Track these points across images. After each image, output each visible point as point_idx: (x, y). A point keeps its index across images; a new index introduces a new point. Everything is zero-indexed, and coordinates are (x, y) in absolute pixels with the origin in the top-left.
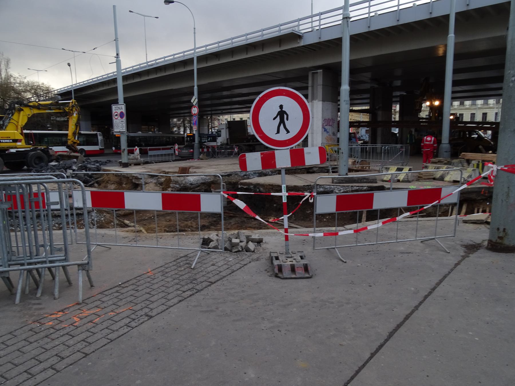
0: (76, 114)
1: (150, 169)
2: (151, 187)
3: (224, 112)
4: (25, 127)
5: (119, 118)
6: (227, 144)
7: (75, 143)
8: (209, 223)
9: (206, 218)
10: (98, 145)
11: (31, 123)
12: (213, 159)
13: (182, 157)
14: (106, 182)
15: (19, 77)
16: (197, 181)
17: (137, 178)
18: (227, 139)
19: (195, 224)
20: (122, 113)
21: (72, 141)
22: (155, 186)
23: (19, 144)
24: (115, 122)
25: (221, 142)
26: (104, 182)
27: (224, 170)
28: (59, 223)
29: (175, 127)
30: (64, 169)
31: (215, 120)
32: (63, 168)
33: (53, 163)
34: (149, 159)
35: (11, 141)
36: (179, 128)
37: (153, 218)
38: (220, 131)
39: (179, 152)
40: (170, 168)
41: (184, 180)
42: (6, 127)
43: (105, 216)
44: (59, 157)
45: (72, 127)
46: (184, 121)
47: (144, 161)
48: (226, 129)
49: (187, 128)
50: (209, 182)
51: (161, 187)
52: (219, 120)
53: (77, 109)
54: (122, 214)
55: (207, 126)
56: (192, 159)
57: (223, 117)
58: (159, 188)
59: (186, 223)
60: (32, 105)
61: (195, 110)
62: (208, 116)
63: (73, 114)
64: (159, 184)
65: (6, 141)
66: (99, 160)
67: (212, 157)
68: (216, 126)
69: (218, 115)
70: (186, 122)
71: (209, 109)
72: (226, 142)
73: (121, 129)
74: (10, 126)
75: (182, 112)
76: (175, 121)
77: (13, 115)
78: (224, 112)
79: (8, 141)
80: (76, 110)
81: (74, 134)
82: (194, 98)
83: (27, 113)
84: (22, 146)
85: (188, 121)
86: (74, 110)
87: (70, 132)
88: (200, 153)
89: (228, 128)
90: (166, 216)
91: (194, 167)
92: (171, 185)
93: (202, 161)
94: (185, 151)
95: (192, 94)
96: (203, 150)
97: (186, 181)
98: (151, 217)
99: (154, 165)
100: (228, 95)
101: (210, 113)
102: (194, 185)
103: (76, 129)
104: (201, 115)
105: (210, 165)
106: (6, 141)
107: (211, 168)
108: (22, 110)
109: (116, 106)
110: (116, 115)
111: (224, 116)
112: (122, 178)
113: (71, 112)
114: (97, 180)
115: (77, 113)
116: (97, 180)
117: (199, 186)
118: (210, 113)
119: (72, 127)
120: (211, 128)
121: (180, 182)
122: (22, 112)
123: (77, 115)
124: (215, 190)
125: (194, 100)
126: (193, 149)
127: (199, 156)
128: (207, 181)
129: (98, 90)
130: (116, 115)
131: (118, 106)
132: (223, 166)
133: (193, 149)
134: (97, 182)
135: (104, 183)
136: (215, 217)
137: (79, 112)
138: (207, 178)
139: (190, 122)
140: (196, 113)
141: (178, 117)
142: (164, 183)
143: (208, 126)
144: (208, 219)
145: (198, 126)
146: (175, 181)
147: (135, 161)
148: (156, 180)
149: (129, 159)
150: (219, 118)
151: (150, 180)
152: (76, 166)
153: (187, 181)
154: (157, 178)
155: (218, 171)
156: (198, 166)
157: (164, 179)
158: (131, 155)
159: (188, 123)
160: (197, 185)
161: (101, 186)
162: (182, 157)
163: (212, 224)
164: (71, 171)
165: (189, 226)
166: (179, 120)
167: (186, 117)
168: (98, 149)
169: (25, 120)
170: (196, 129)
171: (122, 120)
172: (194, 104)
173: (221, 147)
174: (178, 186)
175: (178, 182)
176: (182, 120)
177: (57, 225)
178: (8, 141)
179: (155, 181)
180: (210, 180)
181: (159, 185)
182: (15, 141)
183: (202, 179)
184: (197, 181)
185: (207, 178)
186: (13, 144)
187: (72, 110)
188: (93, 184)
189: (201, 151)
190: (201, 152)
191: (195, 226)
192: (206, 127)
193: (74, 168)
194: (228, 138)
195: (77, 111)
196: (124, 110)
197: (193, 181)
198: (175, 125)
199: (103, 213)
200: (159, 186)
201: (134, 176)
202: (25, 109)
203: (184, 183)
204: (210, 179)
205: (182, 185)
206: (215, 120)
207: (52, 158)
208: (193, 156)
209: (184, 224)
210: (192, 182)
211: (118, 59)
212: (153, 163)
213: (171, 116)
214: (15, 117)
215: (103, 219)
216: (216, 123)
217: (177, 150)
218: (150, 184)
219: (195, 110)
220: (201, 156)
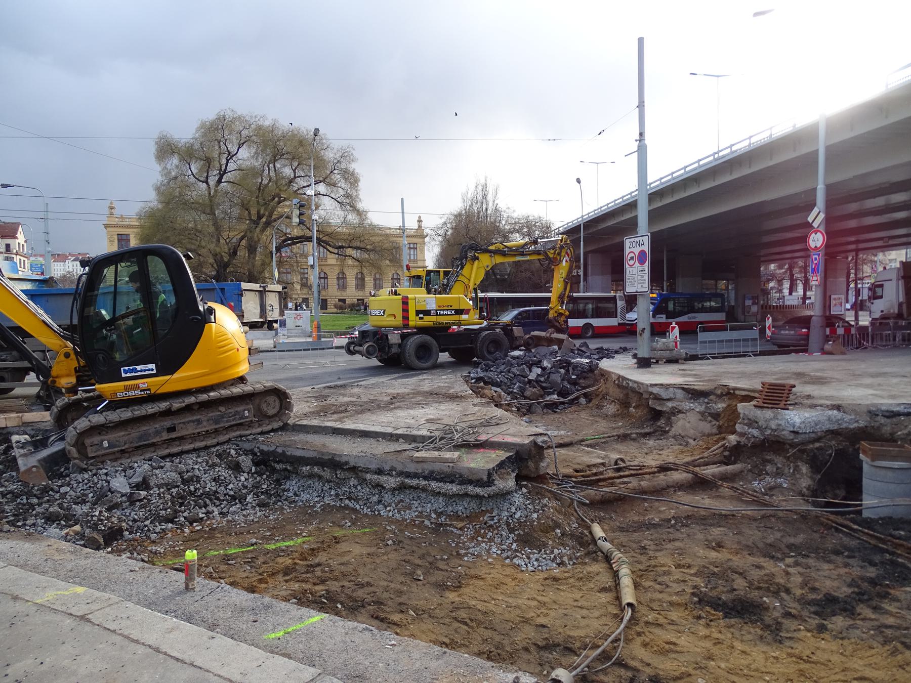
0: (566, 261)
1: (695, 375)
2: (689, 422)
3: (891, 242)
4: (484, 287)
5: (637, 264)
6: (900, 316)
7: (561, 314)
8: (850, 586)
9: (839, 559)
10: (616, 317)
11: (491, 280)
12: (860, 354)
13: (780, 346)
14: (601, 396)
15: (507, 210)
16: (813, 424)
17: (657, 398)
18: (900, 305)
19: (799, 579)
20: (642, 253)
21: (556, 312)
22: (700, 420)
23: (464, 317)
24: (628, 273)
25: (882, 311)
26: (598, 395)
27: (901, 396)
28: (439, 511)
29: (772, 280)
30: (527, 366)
31: (866, 264)
32: (525, 364)
33: (516, 353)
34: (698, 350)
35: (453, 312)
36: (780, 282)
37: (673, 522)
38: (882, 286)
39: (773, 333)
40: (743, 375)
41: (775, 418)
42: (450, 289)
43: (546, 505)
44: (531, 341)
45: (557, 285)
46: (791, 269)
47: (686, 354)
48: (898, 280)
49: (798, 282)
50: (851, 430)
51: (714, 422)
52: (872, 261)
53: (569, 251)
54: (598, 498)
55: (845, 276)
56: (806, 351)
57: (885, 255)
58: (709, 425)
59: (770, 566)
60: (494, 248)
61: (817, 240)
62: (848, 254)
63: (561, 261)
64: (711, 415)
65: (446, 312)
66: (605, 346)
67: (857, 348)
68: (865, 275)
69: (874, 251)
70: (796, 270)
71: (853, 239)
72: (896, 311)
73: (639, 286)
74: (458, 287)
75: (788, 248)
76: (772, 268)
77: (462, 268)
78: (891, 242)
79: (449, 312)
80: (567, 253)
81: (561, 298)
82: (815, 211)
83: (486, 261)
84: (472, 320)
85: (800, 267)
86: (563, 254)
87: (553, 295)
88: (827, 339)
89: (903, 277)
90: (711, 525)
91: (807, 379)
92: (738, 427)
93: (830, 360)
94: (787, 332)
95: (811, 206)
96: (833, 331)
97: (780, 422)
98: (670, 520)
99: (709, 365)
100: (905, 201)
101: (853, 247)
102: (802, 436)
103: (565, 289)
104: (832, 252)
105: (854, 375)
106: (446, 312)
107: (861, 385)
108: (478, 258)
109: (632, 240)
110: (632, 258)
111: (887, 253)
112: (630, 393)
113: (558, 258)
114: (587, 390)
115: (568, 260)
116: (587, 390)
117: (818, 440)
118: (853, 247)
119: (557, 285)
120: (856, 281)
121: (762, 423)
122: (476, 262)
123: (568, 264)
124: (873, 460)
125: (817, 217)
126: (808, 328)
127: (824, 345)
128: (844, 426)
129: (623, 219)
130: (632, 258)
131: (636, 239)
132: (895, 380)
133: (808, 328)
134: (585, 395)
135: (598, 399)
136: (872, 564)
137: (572, 257)
138: (847, 417)
139: (805, 269)
140: (818, 246)
141: (777, 258)
142: (722, 415)
143: (848, 276)
144: (846, 565)
145: (823, 275)
146: (749, 419)
147: (667, 354)
148: (704, 407)
149: (653, 349)
150: (876, 259)
151: (687, 405)
152: (549, 362)
153: (782, 423)
154: (706, 400)
155: (882, 397)
156: (819, 374)
157: (724, 405)
158: (659, 339)
159: (800, 272)
160: (813, 435)
161: (590, 405)
162: (780, 346)
163: (861, 597)
164: (539, 371)
165: (778, 584)
166: (780, 267)
167: (795, 260)
168: (617, 324)
169: (482, 276)
170: (817, 283)
171: (642, 268)
172: (815, 225)
173: (880, 324)
174: (755, 432)
175: (757, 422)
176: (786, 267)
177: (433, 516)
178: (449, 312)
179: (702, 408)
180: (856, 425)
181: (709, 418)
182: (459, 312)
183: (829, 419)
184: (813, 424)
185: (847, 417)
186: (456, 318)
187: (559, 254)
188: (577, 398)
189: (828, 332)
190: (827, 336)
191: (798, 592)
192: (843, 280)
193: (546, 364)
194: (901, 300)
195: (568, 255)
196: (646, 248)
197: (803, 426)
198: (772, 277)
199: (544, 497)
200: (710, 422)
201: (651, 393)
202: (481, 256)
203: (774, 427)
204: (857, 421)
205: (768, 432)
206: (864, 262)
207: (518, 343)
208: (807, 345)
209: (763, 572)
210: (800, 428)
211: (642, 142)
212: (708, 359)
213: (762, 259)
214: (466, 271)
215: (535, 515)
216: (867, 269)
217: (769, 328)
218: (688, 414)
219: (817, 240)
220: (828, 346)
